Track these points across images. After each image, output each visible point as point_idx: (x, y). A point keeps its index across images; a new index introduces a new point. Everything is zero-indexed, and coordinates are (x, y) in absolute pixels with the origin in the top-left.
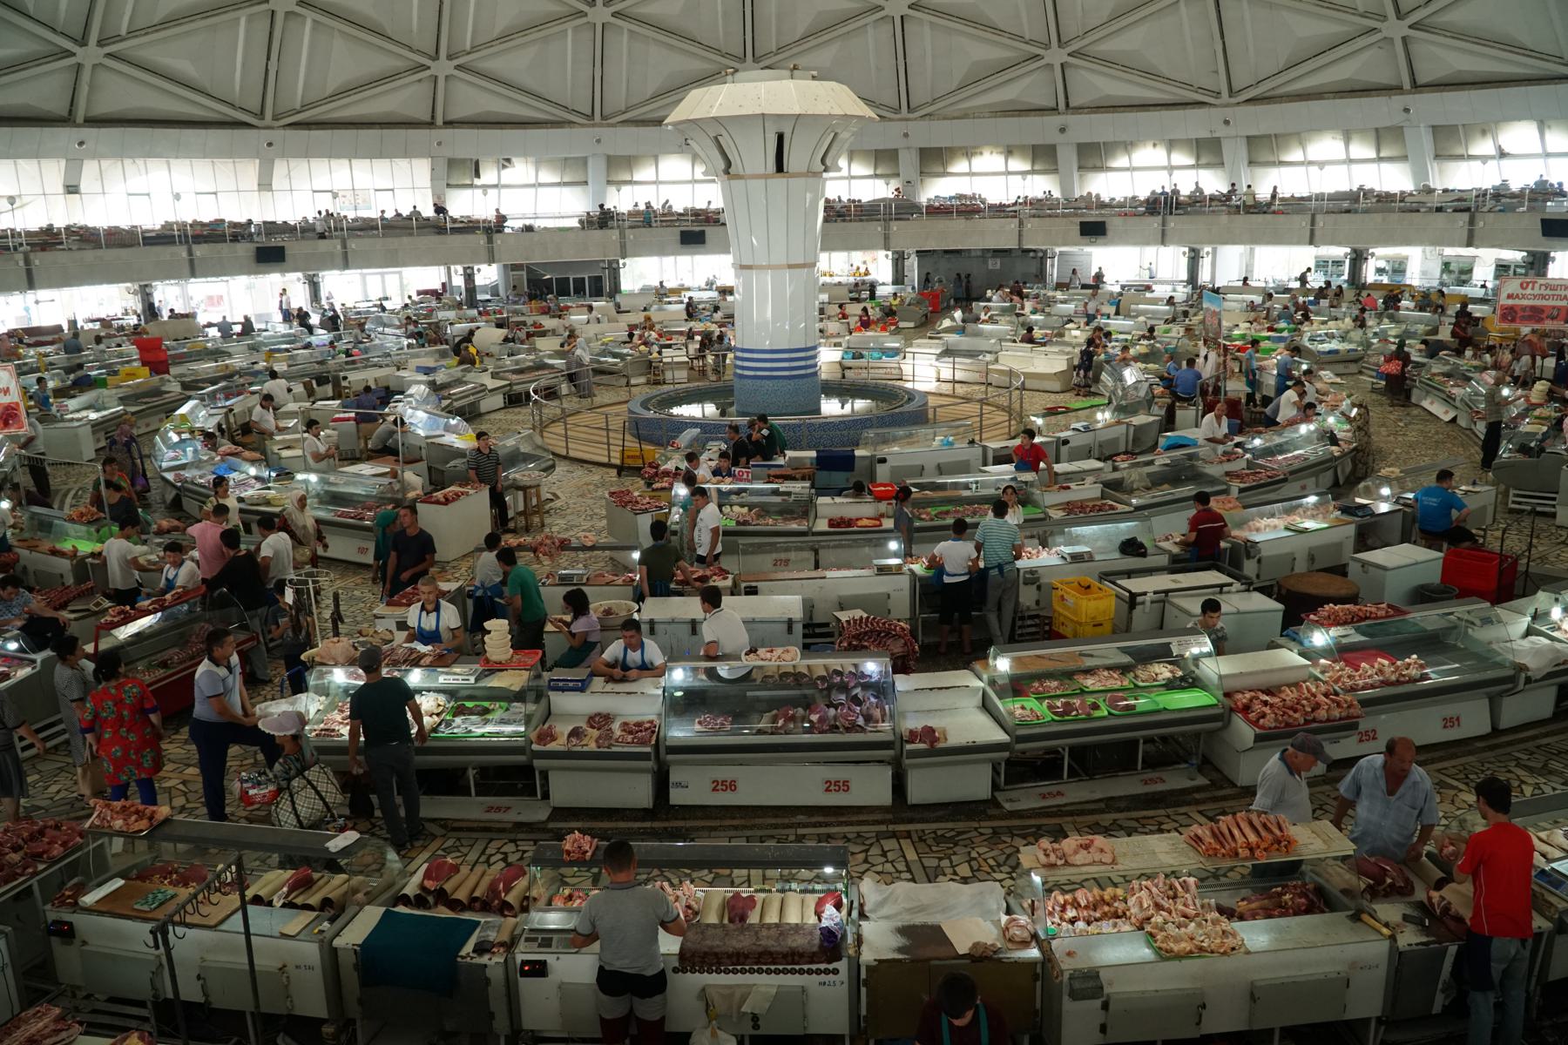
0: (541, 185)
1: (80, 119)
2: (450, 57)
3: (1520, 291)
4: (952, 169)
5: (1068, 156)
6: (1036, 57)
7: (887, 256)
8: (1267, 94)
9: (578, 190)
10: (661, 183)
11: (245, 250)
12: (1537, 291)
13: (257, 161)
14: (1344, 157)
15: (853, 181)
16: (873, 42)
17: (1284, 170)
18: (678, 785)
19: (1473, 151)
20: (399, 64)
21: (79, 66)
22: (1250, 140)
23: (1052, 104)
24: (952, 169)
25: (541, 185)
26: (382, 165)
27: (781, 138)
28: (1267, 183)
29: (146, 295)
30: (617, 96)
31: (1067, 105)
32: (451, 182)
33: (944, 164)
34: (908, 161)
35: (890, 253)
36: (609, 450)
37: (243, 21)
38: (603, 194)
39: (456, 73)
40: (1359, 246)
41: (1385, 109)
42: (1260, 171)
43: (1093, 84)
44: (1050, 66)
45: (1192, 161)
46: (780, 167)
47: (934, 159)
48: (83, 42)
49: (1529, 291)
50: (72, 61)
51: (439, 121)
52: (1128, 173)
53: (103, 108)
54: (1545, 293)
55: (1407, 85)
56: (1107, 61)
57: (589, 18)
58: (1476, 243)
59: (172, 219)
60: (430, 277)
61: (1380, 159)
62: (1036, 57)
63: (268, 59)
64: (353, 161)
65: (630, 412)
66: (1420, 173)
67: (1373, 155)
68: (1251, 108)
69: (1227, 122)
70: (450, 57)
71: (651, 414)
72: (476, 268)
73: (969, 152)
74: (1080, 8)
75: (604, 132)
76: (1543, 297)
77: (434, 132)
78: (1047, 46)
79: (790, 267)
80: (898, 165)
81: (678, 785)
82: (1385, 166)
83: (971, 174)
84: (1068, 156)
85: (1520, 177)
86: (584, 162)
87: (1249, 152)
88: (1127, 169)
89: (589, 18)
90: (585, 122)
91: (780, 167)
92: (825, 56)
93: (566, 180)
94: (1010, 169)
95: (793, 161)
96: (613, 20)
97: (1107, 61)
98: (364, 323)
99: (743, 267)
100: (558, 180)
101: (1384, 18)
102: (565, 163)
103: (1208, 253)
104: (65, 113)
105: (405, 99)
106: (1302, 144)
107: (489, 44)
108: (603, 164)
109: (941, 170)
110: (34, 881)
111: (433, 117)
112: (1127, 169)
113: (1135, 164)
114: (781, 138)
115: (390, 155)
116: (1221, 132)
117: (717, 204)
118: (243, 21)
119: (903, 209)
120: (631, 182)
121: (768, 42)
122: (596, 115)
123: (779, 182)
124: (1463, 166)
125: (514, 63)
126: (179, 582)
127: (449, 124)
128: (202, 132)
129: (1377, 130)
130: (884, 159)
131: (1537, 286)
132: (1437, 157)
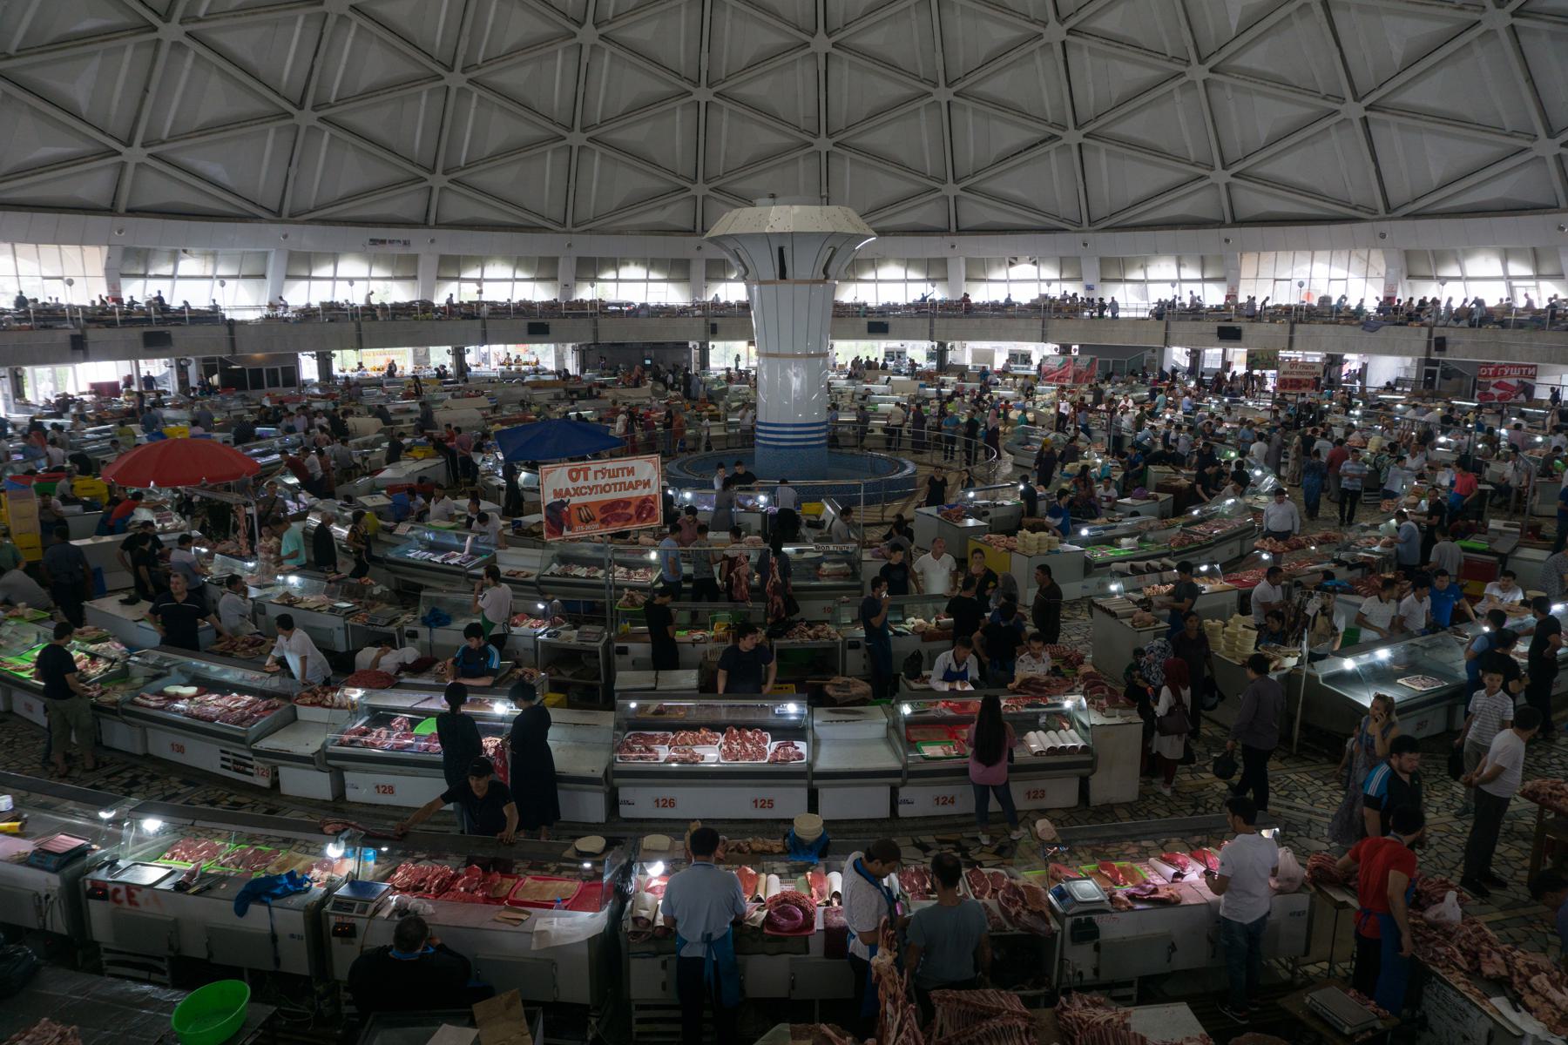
0: (518, 280)
1: (122, 209)
2: (445, 172)
3: (570, 485)
5: (698, 269)
6: (1201, 177)
9: (407, 284)
10: (621, 281)
11: (136, 333)
12: (591, 482)
13: (105, 249)
18: (907, 802)
21: (123, 165)
22: (1102, 260)
23: (944, 226)
24: (993, 276)
25: (518, 280)
26: (49, 250)
27: (781, 250)
28: (981, 294)
29: (459, 355)
31: (1233, 217)
32: (292, 273)
37: (549, 155)
38: (281, 288)
39: (711, 193)
40: (1198, 348)
43: (1254, 201)
44: (1217, 186)
46: (783, 275)
48: (129, 143)
49: (581, 483)
50: (117, 159)
52: (874, 285)
53: (145, 201)
54: (603, 482)
55: (1228, 220)
57: (295, 121)
60: (110, 371)
63: (290, 165)
64: (17, 246)
66: (696, 292)
67: (1057, 276)
68: (1410, 223)
70: (445, 172)
73: (615, 264)
75: (291, 229)
77: (117, 219)
78: (944, 181)
81: (907, 802)
82: (1207, 286)
83: (617, 280)
84: (698, 269)
85: (1024, 295)
86: (943, 262)
87: (1101, 266)
88: (1005, 281)
89: (295, 121)
90: (273, 218)
91: (783, 275)
93: (1064, 276)
94: (1183, 277)
99: (768, 355)
100: (235, 273)
101: (1065, 128)
104: (109, 207)
105: (92, 184)
106: (1144, 267)
107: (186, 136)
108: (435, 261)
110: (354, 913)
112: (1005, 281)
113: (879, 277)
114: (781, 250)
115: (57, 240)
118: (549, 155)
122: (567, 222)
123: (784, 288)
124: (983, 286)
125: (501, 178)
127: (132, 212)
128: (81, 218)
131: (591, 474)
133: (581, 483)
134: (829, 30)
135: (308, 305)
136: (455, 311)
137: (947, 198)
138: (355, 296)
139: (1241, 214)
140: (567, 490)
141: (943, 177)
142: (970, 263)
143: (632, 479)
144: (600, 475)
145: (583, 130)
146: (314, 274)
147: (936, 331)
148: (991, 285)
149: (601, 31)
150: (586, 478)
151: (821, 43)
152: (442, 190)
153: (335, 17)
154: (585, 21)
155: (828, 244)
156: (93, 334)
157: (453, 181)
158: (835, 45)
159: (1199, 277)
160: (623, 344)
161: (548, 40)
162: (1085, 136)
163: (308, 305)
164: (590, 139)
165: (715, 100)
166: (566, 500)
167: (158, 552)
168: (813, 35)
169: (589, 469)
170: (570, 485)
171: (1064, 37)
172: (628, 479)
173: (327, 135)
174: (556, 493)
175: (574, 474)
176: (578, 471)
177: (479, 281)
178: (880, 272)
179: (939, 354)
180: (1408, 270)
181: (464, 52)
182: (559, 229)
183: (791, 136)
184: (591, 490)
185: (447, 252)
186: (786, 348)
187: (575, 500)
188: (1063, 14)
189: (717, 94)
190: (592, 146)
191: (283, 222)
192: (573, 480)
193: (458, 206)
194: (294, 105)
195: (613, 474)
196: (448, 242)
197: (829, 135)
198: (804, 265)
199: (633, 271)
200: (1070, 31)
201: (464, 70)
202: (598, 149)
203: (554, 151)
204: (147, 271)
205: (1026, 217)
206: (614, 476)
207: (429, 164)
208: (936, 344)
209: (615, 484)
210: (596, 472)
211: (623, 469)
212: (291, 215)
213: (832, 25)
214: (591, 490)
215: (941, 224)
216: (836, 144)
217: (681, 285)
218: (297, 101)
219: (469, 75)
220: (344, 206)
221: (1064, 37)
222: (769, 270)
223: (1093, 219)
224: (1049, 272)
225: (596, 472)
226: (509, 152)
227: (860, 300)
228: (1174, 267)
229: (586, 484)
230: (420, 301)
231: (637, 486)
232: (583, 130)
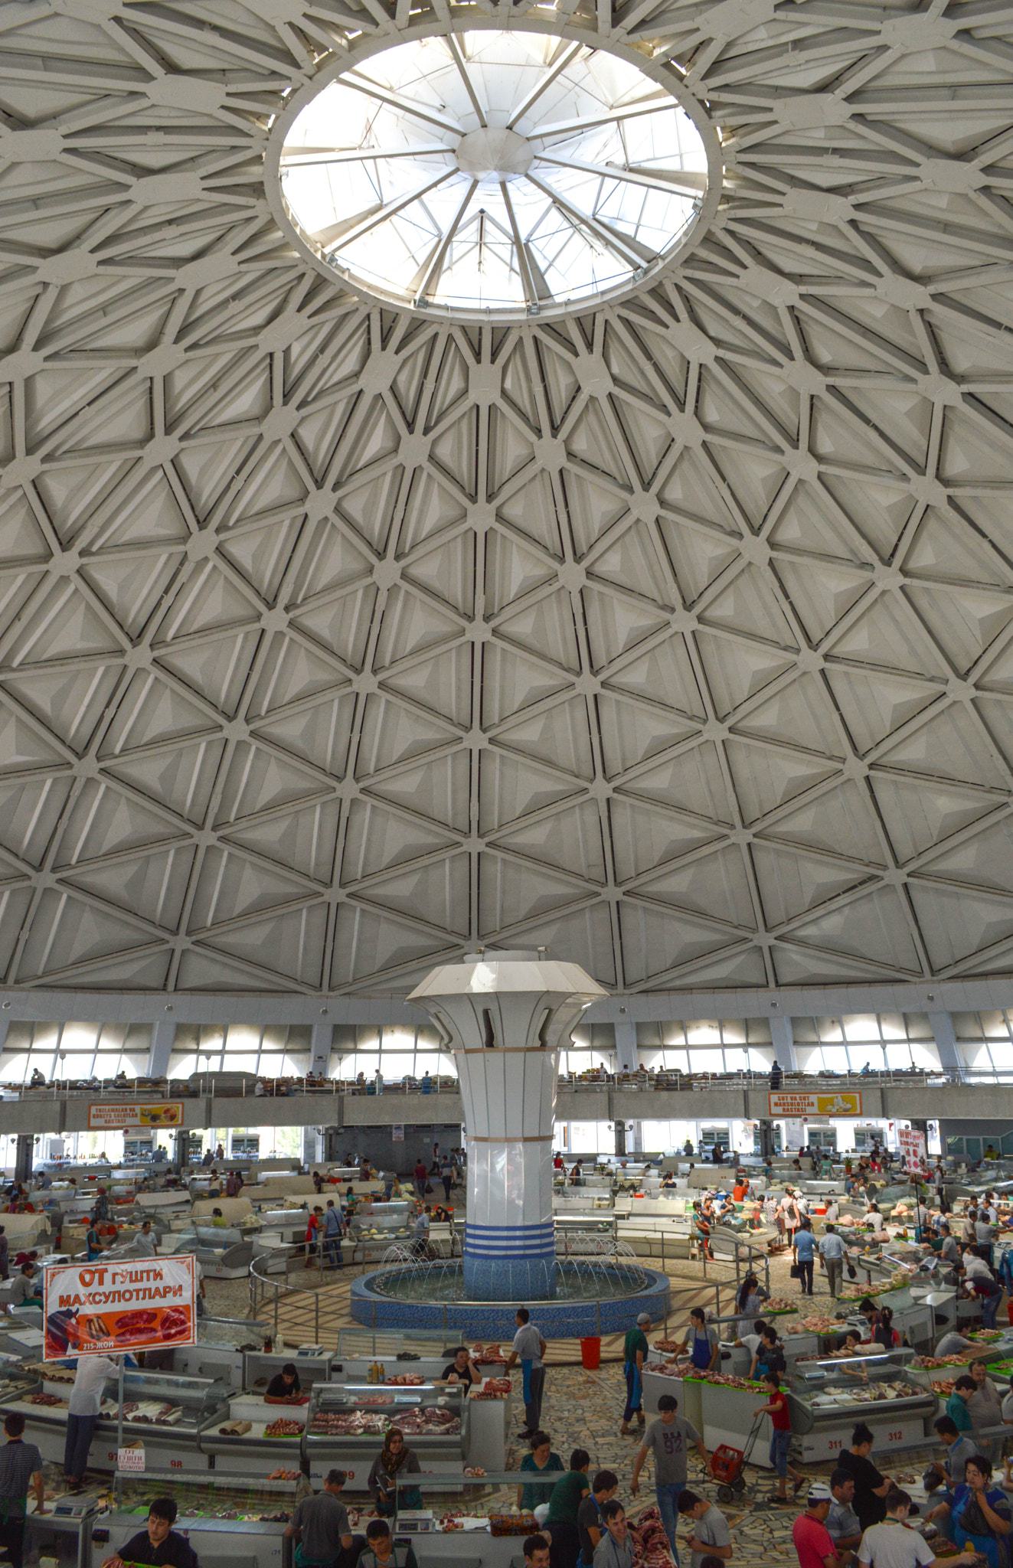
4: (205, 1045)
5: (625, 1035)
6: (745, 940)
7: (610, 1127)
8: (968, 973)
12: (108, 1287)
14: (412, 1047)
15: (727, 1051)
16: (592, 926)
17: (667, 1053)
19: (826, 1038)
20: (136, 936)
24: (826, 1038)
27: (486, 1013)
28: (813, 1062)
30: (348, 965)
33: (355, 1041)
34: (321, 1035)
35: (613, 1124)
36: (317, 1332)
37: (304, 912)
41: (754, 1002)
42: (645, 1053)
45: (903, 1035)
46: (490, 1042)
47: (345, 1037)
49: (95, 1288)
51: (171, 986)
56: (802, 942)
58: (213, 1123)
59: (823, 1069)
61: (909, 1041)
62: (745, 940)
65: (354, 1293)
69: (623, 1011)
70: (189, 933)
71: (375, 1297)
72: (36, 1136)
74: (498, 907)
76: (120, 1296)
78: (755, 930)
79: (526, 1140)
80: (614, 1037)
82: (915, 1047)
85: (858, 1060)
87: (638, 1034)
92: (545, 936)
94: (418, 1047)
95: (550, 1038)
96: (347, 900)
97: (802, 942)
98: (424, 1190)
102: (746, 1026)
103: (631, 1127)
109: (351, 1046)
111: (165, 985)
114: (486, 1013)
116: (616, 1019)
117: (453, 1073)
118: (304, 912)
119: (316, 1084)
120: (29, 1051)
121: (493, 921)
123: (495, 1058)
124: (817, 1051)
126: (256, 1518)
129: (746, 1020)
130: (601, 1034)
131: (108, 1277)
132: (795, 1043)
133: (95, 1288)
134: (609, 775)
135: (122, 1076)
136: (187, 1090)
137: (761, 948)
138: (75, 1070)
139: (786, 976)
140: (77, 1297)
141: (753, 926)
142: (640, 1027)
143: (159, 1284)
144: (119, 1279)
145: (342, 885)
146: (36, 1046)
147: (752, 1107)
148: (825, 1049)
149: (361, 785)
150: (101, 1282)
151: (601, 789)
152: (184, 952)
153: (83, 780)
154: (345, 776)
155: (541, 1006)
156: (219, 1103)
157: (196, 943)
158: (616, 790)
159: (904, 1037)
160: (429, 1126)
161: (308, 794)
162: (909, 875)
163: (95, 1079)
164: (350, 895)
165: (488, 850)
166: (74, 1309)
167: (518, 1360)
168: (592, 781)
169: (106, 1270)
170: (82, 1291)
171: (867, 772)
172: (152, 1284)
173: (65, 896)
174: (63, 1301)
175: (87, 1277)
176: (92, 1273)
177: (222, 1052)
178: (848, 1028)
179: (186, 1143)
180: (638, 1040)
181: (216, 810)
182: (917, 979)
183: (578, 886)
184: (107, 1298)
185: (182, 1020)
186: (498, 1132)
187: (88, 1310)
188: (862, 749)
189: (489, 844)
190: (353, 902)
191: (10, 989)
192: (85, 1284)
193: (202, 969)
194: (34, 867)
195: (135, 1277)
196: (187, 1008)
197: (617, 884)
198: (515, 1030)
199: (704, 1033)
200: (872, 766)
201: (214, 828)
202: (359, 905)
203: (310, 908)
204: (356, 1045)
205: (863, 970)
206: (136, 1280)
207: (173, 926)
208: (757, 1122)
209: (138, 1291)
210: (114, 1275)
211: (148, 1272)
212: (17, 982)
213: (611, 772)
214: (107, 1298)
215: (756, 977)
216: (626, 893)
217: (301, 1056)
218: (37, 864)
219: (220, 833)
220: (68, 973)
221: (867, 772)
222: (474, 1037)
223: (936, 967)
224: (893, 1031)
225: (114, 1275)
226: (260, 908)
227: (670, 1066)
228: (94, 1037)
229: (101, 1289)
230: (139, 1078)
231: (165, 1293)
232: (342, 885)
